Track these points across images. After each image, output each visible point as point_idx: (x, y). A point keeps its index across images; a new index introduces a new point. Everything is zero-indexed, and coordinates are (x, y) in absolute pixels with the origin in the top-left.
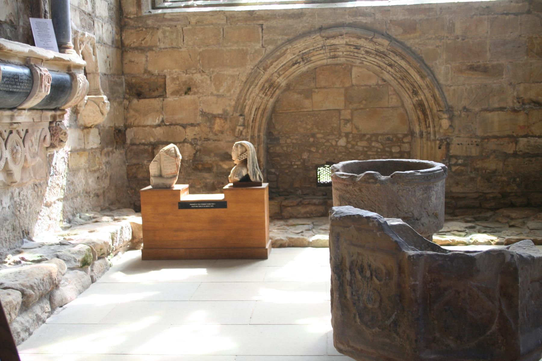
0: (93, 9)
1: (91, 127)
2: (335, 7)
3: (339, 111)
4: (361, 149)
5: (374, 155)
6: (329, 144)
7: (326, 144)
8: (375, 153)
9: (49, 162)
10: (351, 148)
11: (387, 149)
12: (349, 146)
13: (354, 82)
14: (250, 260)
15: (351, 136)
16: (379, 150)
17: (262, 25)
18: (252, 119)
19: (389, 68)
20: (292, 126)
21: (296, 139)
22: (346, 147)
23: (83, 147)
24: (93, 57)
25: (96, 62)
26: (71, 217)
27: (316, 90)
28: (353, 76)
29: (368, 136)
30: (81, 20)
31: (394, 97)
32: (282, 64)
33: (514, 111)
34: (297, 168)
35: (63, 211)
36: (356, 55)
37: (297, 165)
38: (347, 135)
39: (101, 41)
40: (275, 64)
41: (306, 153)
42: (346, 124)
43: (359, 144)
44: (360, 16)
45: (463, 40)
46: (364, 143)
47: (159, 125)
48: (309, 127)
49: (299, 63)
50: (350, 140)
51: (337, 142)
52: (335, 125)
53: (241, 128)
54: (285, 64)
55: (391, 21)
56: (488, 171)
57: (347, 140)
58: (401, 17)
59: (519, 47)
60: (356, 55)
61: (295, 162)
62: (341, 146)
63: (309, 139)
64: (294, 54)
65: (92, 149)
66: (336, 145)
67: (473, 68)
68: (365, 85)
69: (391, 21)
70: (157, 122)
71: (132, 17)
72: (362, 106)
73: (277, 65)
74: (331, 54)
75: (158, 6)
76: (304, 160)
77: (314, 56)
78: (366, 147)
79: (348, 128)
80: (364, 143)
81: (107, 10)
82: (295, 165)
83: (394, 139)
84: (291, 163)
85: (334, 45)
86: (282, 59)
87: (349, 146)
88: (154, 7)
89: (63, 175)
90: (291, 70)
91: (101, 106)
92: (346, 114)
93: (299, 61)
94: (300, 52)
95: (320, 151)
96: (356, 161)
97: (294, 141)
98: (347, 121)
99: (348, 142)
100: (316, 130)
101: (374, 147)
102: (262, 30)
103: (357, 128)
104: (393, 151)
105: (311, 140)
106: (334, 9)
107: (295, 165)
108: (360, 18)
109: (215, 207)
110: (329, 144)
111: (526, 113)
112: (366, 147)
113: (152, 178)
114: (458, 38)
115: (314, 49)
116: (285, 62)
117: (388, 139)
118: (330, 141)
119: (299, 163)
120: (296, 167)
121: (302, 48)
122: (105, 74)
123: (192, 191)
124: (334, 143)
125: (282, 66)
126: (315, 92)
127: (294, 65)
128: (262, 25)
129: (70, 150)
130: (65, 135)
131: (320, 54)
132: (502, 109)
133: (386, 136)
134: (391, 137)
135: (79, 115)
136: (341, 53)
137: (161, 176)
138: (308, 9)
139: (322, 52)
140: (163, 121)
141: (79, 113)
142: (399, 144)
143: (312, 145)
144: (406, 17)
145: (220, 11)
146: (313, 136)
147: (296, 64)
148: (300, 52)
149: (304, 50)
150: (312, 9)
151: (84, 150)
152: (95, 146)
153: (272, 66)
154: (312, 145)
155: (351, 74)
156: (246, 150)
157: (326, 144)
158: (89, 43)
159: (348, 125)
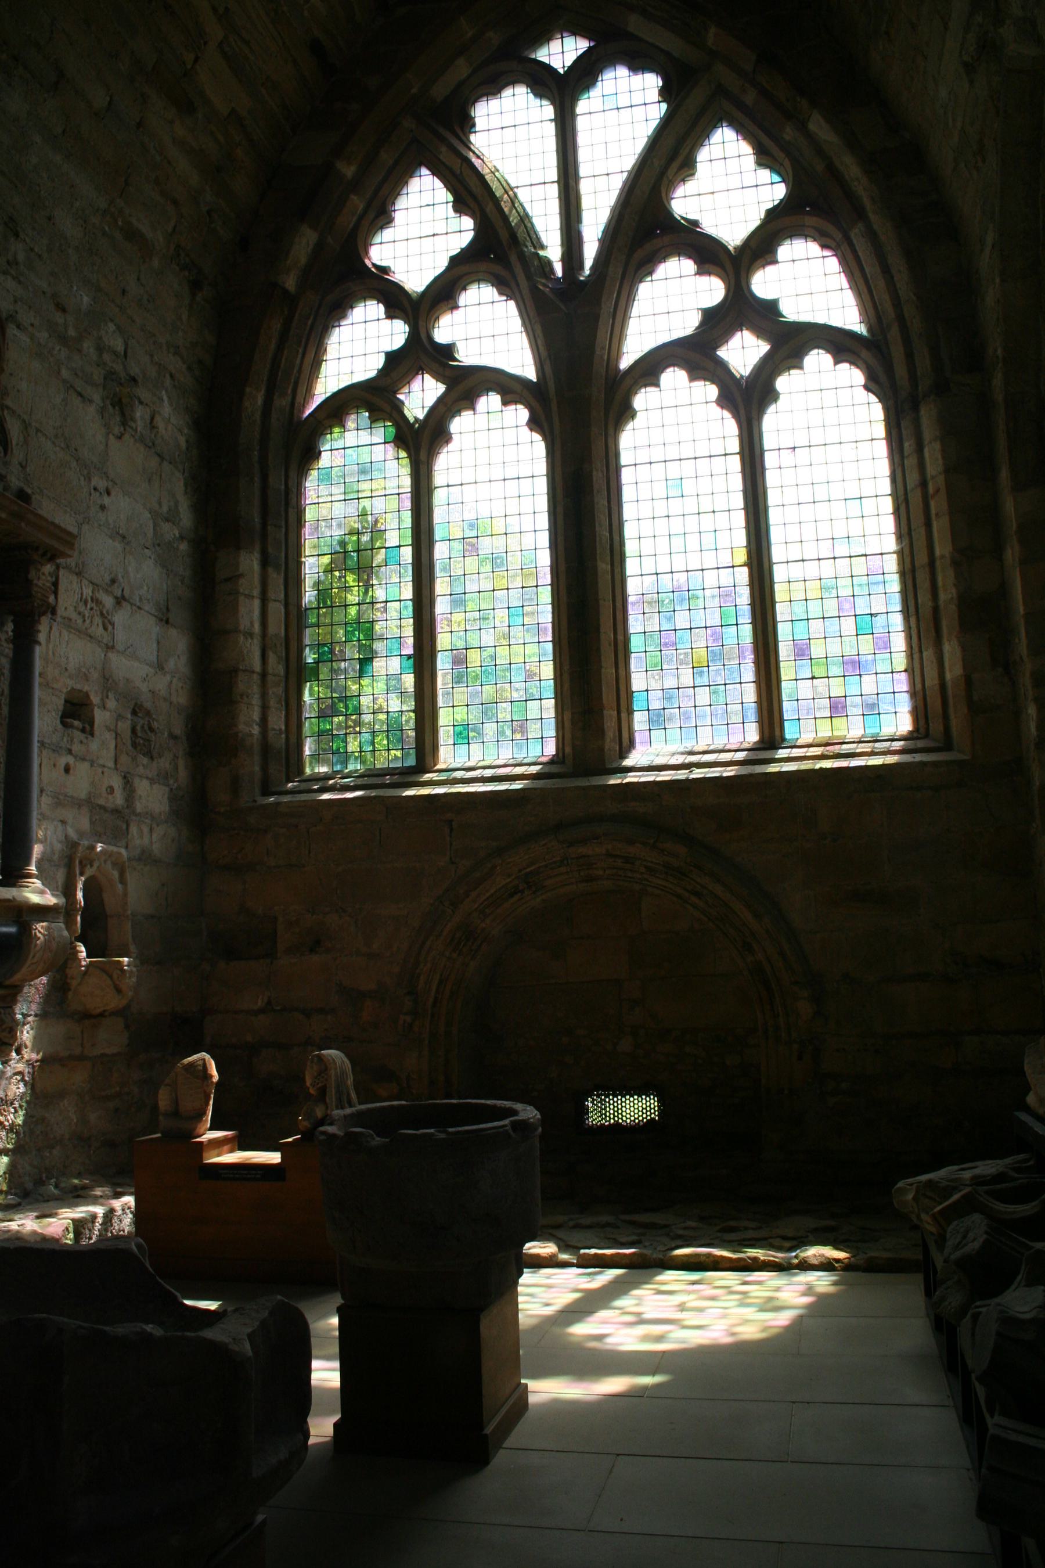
0: (127, 800)
1: (102, 1015)
2: (588, 784)
14: (654, 1270)
17: (451, 821)
18: (431, 1000)
19: (694, 899)
23: (78, 1051)
24: (120, 886)
25: (125, 894)
26: (29, 1186)
30: (92, 823)
32: (488, 895)
35: (11, 1175)
36: (629, 874)
39: (145, 857)
47: (262, 1011)
49: (522, 891)
53: (408, 1019)
54: (492, 895)
60: (629, 874)
65: (103, 1055)
70: (260, 1004)
71: (222, 810)
74: (582, 874)
75: (274, 790)
81: (166, 800)
85: (584, 856)
88: (266, 793)
89: (17, 1105)
91: (115, 977)
93: (521, 888)
94: (520, 871)
96: (403, 1102)
102: (451, 830)
106: (584, 788)
113: (161, 1118)
115: (546, 866)
116: (492, 891)
122: (152, 917)
123: (432, 1134)
127: (511, 896)
128: (451, 821)
129: (40, 1057)
130: (10, 1032)
135: (70, 995)
136: (601, 873)
137: (176, 1114)
138: (535, 789)
139: (563, 869)
140: (269, 1003)
141: (69, 990)
145: (375, 797)
147: (515, 893)
148: (520, 871)
150: (542, 789)
151: (81, 1058)
152: (113, 1050)
156: (326, 1069)
158: (109, 862)
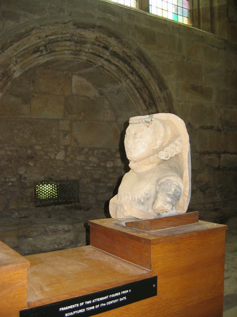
3: (58, 120)
4: (79, 163)
5: (90, 170)
6: (47, 158)
7: (44, 157)
8: (91, 168)
9: (51, 179)
10: (70, 163)
11: (102, 164)
12: (68, 160)
13: (74, 91)
15: (70, 149)
16: (95, 165)
20: (8, 134)
21: (11, 151)
22: (64, 161)
27: (36, 95)
28: (73, 85)
29: (86, 150)
31: (109, 111)
33: (219, 130)
34: (12, 186)
37: (11, 182)
38: (66, 148)
40: (15, 45)
41: (23, 168)
42: (65, 135)
43: (78, 158)
44: (109, 13)
45: (188, 60)
46: (82, 158)
48: (26, 137)
50: (68, 154)
51: (56, 155)
52: (54, 136)
54: (27, 48)
55: (135, 26)
56: (204, 183)
57: (66, 153)
58: (143, 25)
59: (221, 76)
61: (9, 178)
62: (59, 160)
63: (27, 151)
64: (40, 38)
66: (55, 159)
67: (194, 88)
68: (85, 96)
69: (135, 26)
72: (80, 118)
73: (18, 46)
76: (21, 176)
77: (58, 46)
78: (84, 162)
79: (67, 140)
80: (82, 158)
82: (9, 182)
83: (108, 154)
84: (6, 179)
86: (24, 40)
87: (68, 160)
90: (31, 58)
92: (64, 125)
93: (41, 49)
94: (47, 36)
95: (38, 165)
97: (9, 153)
98: (66, 133)
99: (66, 156)
100: (35, 141)
101: (91, 161)
103: (76, 141)
104: (108, 166)
105: (29, 152)
107: (9, 182)
108: (109, 15)
109: (131, 299)
110: (47, 158)
111: (225, 133)
112: (84, 162)
114: (185, 58)
116: (27, 46)
117: (103, 154)
118: (49, 154)
119: (14, 179)
120: (11, 184)
121: (49, 33)
124: (53, 157)
125: (24, 50)
126: (33, 96)
131: (65, 46)
132: (212, 128)
133: (101, 151)
134: (106, 151)
142: (113, 159)
143: (31, 158)
144: (148, 27)
146: (31, 147)
147: (37, 51)
148: (47, 36)
149: (52, 35)
153: (11, 48)
154: (31, 158)
155: (71, 83)
157: (44, 157)
159: (68, 137)
